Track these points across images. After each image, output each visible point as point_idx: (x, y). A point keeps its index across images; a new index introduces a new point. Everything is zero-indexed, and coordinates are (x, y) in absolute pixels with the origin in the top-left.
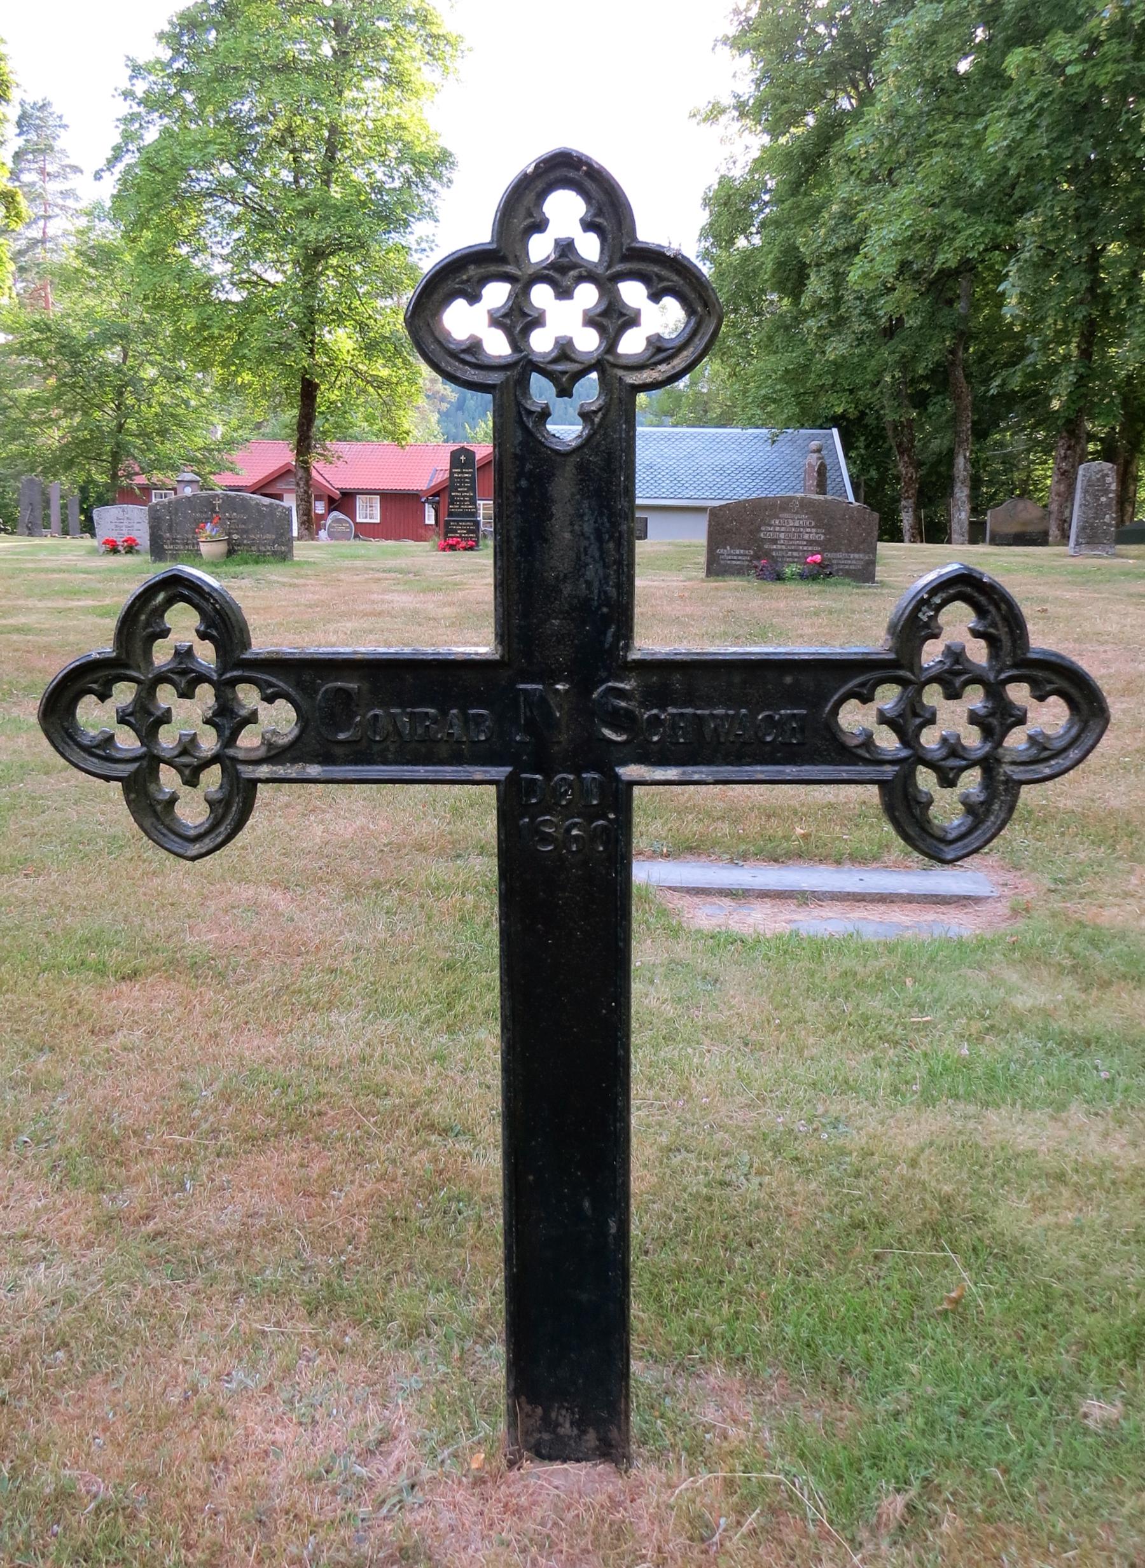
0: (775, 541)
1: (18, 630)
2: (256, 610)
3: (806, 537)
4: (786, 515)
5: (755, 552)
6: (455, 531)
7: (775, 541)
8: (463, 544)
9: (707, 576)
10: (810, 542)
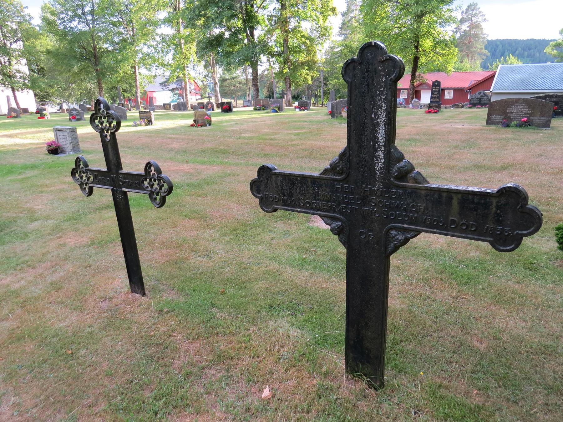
0: (512, 113)
1: (271, 139)
2: (122, 147)
3: (524, 112)
4: (517, 104)
5: (504, 117)
6: (432, 107)
7: (512, 113)
8: (433, 111)
9: (487, 123)
10: (525, 114)
